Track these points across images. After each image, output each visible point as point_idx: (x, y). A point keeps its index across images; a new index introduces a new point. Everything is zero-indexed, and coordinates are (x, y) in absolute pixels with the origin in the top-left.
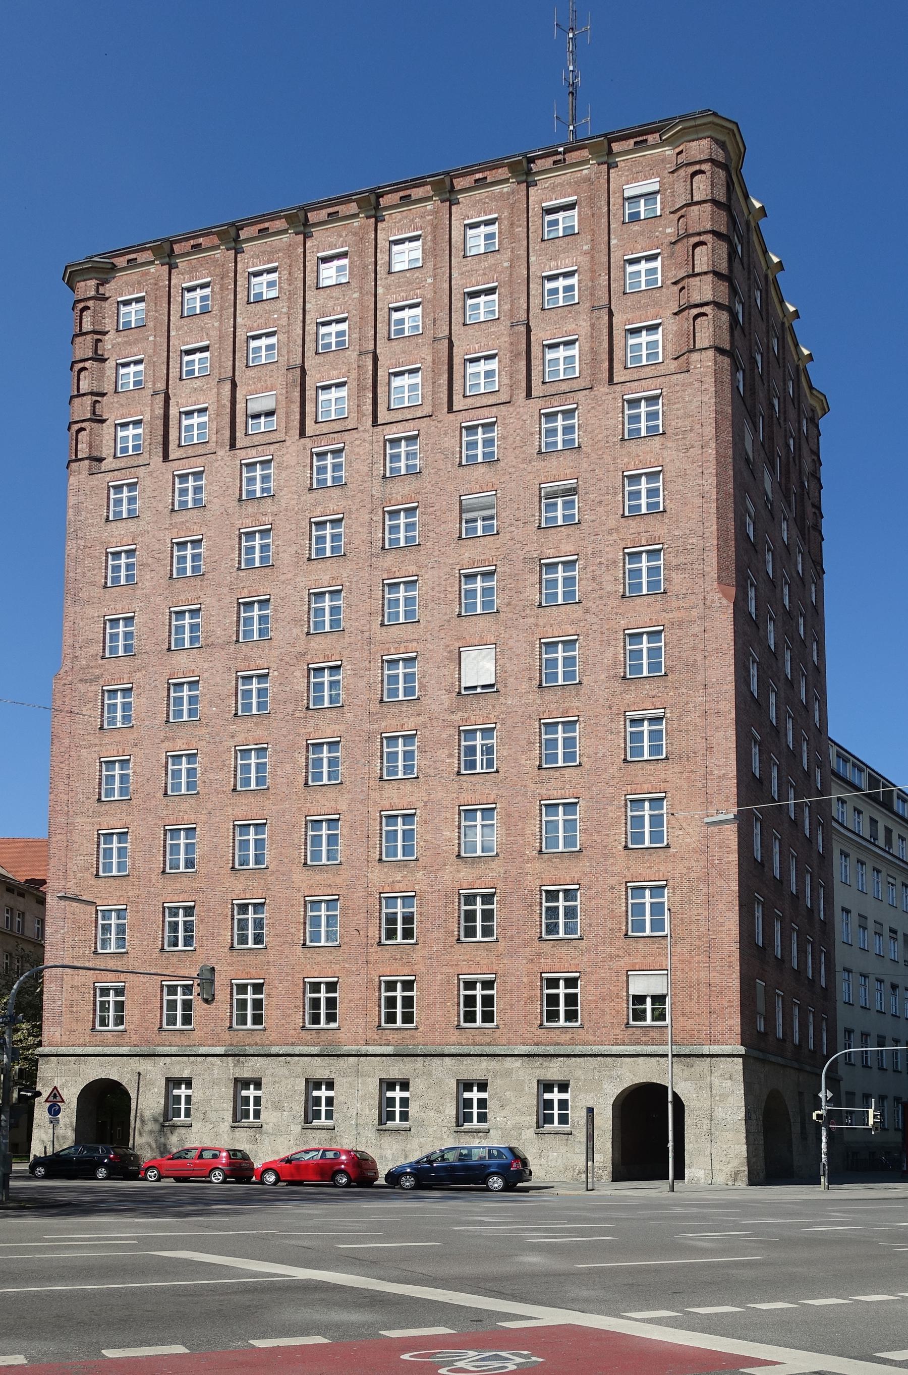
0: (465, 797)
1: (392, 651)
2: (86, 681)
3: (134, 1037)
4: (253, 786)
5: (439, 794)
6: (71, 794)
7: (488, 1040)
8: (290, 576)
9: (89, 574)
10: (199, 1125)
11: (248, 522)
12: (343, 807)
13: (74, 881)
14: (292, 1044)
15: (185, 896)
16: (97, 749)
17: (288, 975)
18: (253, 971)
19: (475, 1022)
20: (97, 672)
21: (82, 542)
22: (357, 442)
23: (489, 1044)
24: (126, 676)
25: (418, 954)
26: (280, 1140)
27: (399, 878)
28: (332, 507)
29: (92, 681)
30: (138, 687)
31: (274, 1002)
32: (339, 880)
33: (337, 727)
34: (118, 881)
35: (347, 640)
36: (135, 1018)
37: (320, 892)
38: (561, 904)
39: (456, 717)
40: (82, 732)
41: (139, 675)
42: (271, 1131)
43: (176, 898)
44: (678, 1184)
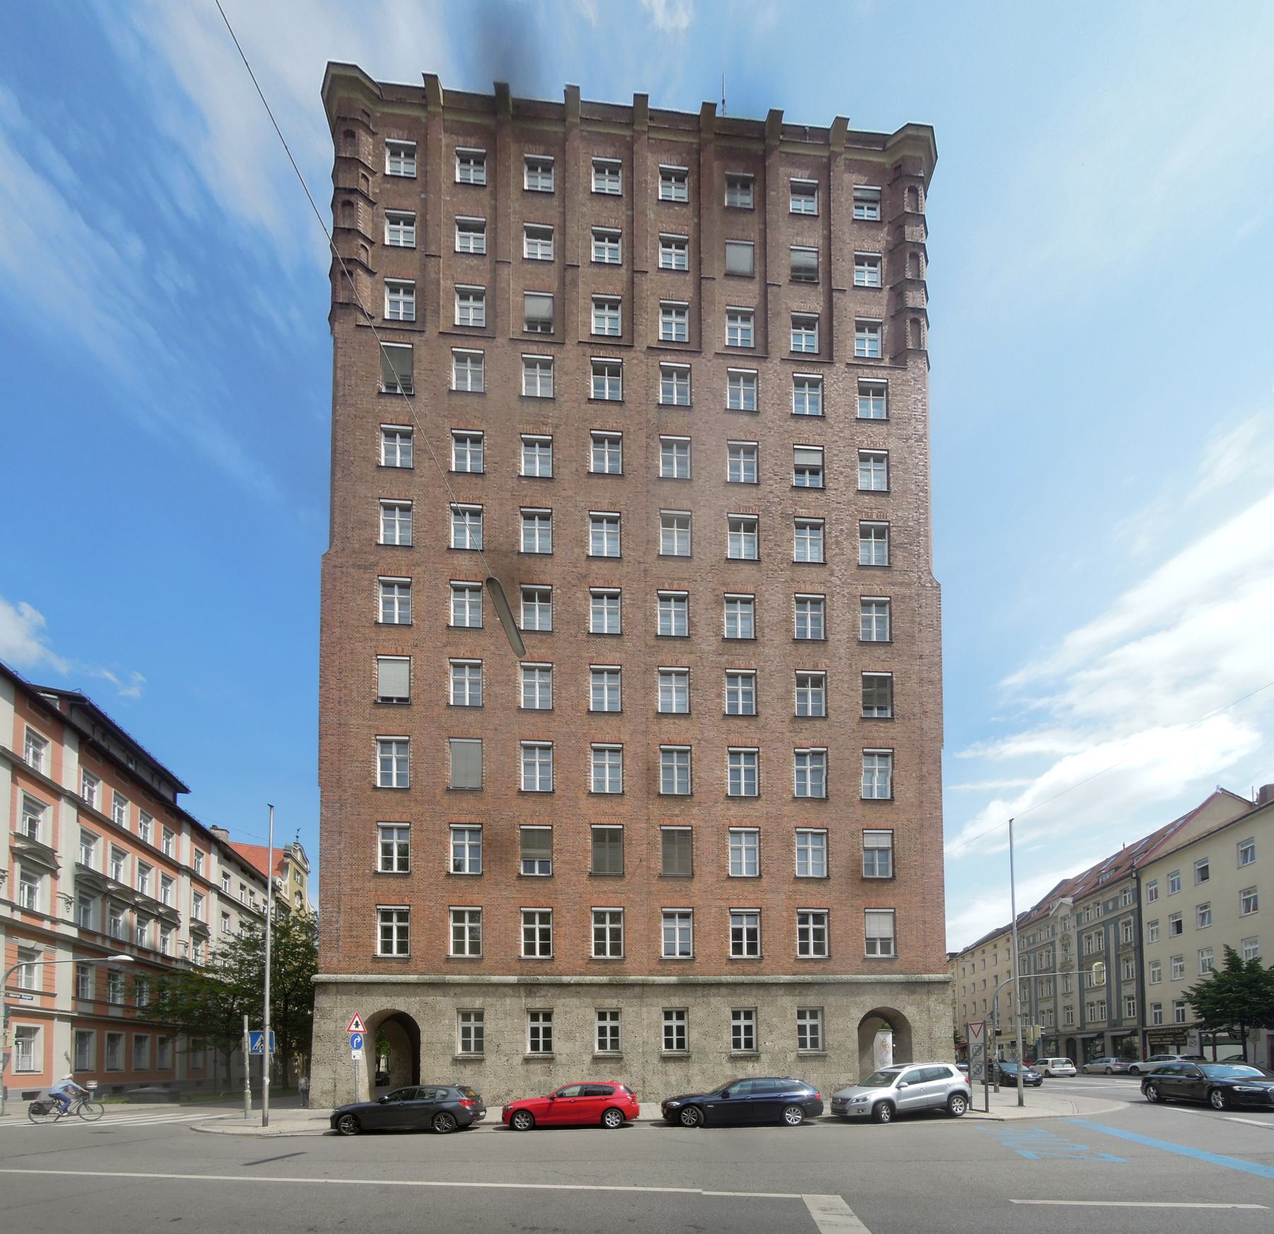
0: (734, 739)
1: (667, 586)
2: (359, 567)
3: (421, 966)
4: (395, 869)
5: (710, 734)
6: (344, 691)
7: (755, 970)
8: (570, 493)
9: (361, 448)
10: (493, 1058)
11: (529, 428)
12: (626, 738)
13: (350, 791)
14: (581, 974)
15: (472, 818)
16: (373, 644)
17: (576, 904)
18: (542, 900)
19: (874, 952)
20: (372, 558)
21: (352, 410)
22: (635, 361)
23: (756, 974)
24: (404, 568)
25: (696, 886)
26: (574, 1070)
27: (677, 812)
28: (611, 423)
29: (366, 568)
30: (418, 582)
31: (562, 931)
32: (622, 810)
33: (618, 655)
34: (399, 795)
35: (625, 569)
36: (422, 945)
37: (606, 821)
38: (467, 925)
39: (724, 659)
40: (356, 623)
41: (419, 570)
42: (564, 1061)
43: (463, 819)
44: (724, 1057)
